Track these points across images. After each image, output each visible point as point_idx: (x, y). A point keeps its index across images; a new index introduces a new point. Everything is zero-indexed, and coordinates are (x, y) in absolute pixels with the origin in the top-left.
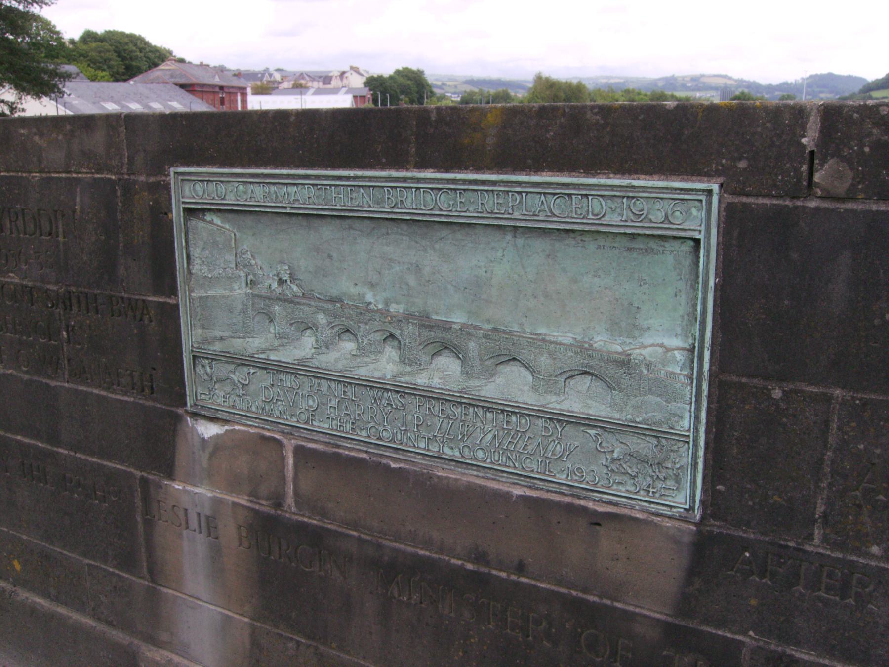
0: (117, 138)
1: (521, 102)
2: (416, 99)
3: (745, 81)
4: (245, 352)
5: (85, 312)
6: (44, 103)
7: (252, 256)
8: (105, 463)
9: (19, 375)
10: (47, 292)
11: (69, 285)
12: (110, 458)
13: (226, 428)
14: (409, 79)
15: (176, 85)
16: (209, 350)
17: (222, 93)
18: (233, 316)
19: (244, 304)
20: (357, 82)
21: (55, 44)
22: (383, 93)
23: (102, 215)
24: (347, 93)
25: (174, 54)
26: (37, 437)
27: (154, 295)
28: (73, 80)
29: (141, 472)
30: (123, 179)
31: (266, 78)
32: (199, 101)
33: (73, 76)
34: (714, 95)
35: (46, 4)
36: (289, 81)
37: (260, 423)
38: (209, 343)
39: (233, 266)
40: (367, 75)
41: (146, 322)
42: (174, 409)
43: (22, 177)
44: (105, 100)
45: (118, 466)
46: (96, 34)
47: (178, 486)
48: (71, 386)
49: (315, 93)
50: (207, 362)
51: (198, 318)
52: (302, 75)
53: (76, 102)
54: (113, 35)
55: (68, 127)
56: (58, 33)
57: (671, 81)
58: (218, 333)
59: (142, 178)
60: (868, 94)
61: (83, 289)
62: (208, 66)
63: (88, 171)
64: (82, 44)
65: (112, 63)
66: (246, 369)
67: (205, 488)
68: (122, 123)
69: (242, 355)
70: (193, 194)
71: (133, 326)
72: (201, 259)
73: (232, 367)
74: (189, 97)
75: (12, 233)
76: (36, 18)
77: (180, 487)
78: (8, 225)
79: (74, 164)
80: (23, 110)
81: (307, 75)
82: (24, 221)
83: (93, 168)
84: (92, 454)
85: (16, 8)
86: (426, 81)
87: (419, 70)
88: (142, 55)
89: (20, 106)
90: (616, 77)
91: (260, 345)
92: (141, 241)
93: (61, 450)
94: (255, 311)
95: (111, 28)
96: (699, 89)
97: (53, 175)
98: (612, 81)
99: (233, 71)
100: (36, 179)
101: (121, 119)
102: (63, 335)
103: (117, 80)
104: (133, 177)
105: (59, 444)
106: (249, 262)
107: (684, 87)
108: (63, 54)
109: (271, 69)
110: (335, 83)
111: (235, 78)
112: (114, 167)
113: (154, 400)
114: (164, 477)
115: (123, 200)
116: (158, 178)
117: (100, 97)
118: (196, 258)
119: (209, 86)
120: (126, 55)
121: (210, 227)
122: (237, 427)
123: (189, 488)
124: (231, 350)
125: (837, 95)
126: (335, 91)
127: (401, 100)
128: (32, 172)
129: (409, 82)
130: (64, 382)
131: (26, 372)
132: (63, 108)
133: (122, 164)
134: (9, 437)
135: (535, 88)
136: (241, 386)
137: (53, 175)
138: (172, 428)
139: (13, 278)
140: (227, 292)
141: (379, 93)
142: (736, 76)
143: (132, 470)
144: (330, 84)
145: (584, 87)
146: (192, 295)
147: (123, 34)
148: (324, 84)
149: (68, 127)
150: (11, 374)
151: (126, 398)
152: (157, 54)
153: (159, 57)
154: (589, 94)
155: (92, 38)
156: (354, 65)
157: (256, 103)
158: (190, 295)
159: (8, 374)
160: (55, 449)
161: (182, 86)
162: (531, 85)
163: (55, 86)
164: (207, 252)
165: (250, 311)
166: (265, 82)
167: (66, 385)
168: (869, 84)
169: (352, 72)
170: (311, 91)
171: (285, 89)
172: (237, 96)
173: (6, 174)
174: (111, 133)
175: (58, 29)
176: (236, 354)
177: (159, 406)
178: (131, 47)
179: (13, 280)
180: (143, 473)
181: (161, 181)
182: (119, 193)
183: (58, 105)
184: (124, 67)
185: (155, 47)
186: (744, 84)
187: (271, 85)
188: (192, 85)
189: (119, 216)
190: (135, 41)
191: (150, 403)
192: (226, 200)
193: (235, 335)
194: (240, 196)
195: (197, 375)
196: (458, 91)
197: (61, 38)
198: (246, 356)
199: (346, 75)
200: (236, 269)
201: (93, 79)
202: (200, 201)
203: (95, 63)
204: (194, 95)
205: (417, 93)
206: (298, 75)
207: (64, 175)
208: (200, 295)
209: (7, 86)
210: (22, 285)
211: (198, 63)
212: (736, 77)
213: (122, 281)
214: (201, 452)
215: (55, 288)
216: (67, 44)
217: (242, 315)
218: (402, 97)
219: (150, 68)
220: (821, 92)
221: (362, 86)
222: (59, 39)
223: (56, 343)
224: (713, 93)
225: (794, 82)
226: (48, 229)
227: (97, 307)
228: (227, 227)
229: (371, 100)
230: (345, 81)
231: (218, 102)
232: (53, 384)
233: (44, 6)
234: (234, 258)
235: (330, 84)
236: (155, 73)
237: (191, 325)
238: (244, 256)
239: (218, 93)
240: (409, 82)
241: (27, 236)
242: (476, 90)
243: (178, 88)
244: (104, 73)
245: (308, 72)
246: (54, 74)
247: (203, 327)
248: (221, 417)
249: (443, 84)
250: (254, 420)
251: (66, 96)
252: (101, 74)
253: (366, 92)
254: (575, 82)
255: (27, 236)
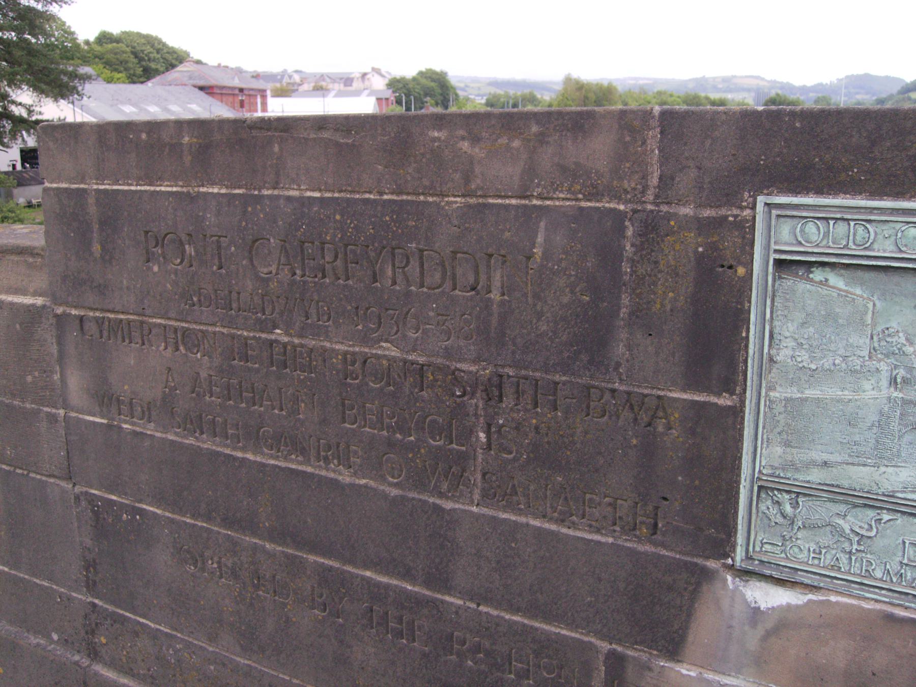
0: (641, 146)
1: (550, 105)
2: (440, 102)
3: (779, 82)
4: (875, 487)
5: (529, 407)
6: (61, 108)
7: (907, 339)
8: (537, 625)
9: (382, 488)
10: (453, 373)
11: (503, 366)
12: (548, 617)
13: (811, 596)
14: (433, 80)
15: (195, 86)
16: (794, 479)
17: (242, 96)
18: (856, 430)
19: (881, 413)
20: (379, 84)
21: (70, 45)
22: (408, 95)
23: (589, 264)
24: (368, 95)
25: (191, 56)
26: (407, 574)
27: (684, 390)
28: (93, 82)
29: (611, 644)
30: (644, 211)
31: (286, 80)
32: (219, 103)
33: (93, 77)
34: (747, 96)
35: (66, 3)
36: (309, 83)
37: (893, 598)
38: (797, 470)
39: (865, 353)
40: (390, 77)
41: (660, 429)
42: (699, 561)
43: (426, 203)
44: (122, 103)
45: (564, 632)
46: (112, 34)
47: (685, 670)
48: (485, 511)
49: (336, 96)
50: (787, 496)
51: (778, 430)
52: (322, 77)
53: (94, 105)
54: (129, 36)
55: (535, 129)
56: (73, 33)
57: (701, 82)
58: (819, 456)
59: (687, 211)
60: (906, 95)
61: (531, 374)
62: (227, 67)
63: (573, 197)
64: (96, 46)
65: (130, 65)
66: (871, 513)
67: (745, 679)
68: (655, 123)
69: (868, 492)
70: (800, 239)
71: (630, 433)
72: (796, 340)
73: (842, 508)
74: (208, 100)
75: (394, 283)
76: (52, 18)
77: (692, 674)
78: (389, 272)
79: (538, 185)
80: (40, 113)
81: (328, 76)
82: (422, 265)
83: (580, 192)
84: (516, 610)
85: (33, 8)
86: (448, 82)
87: (442, 72)
88: (159, 56)
89: (37, 109)
90: (645, 79)
91: (909, 479)
92: (668, 307)
93: (448, 598)
94: (906, 426)
95: (127, 29)
96: (730, 91)
97: (491, 201)
98: (641, 82)
99: (250, 72)
100: (455, 206)
101: (653, 117)
102: (477, 437)
103: (134, 82)
104: (664, 208)
105: (449, 590)
106: (899, 349)
107: (715, 89)
108: (78, 55)
109: (290, 71)
110: (356, 85)
111: (254, 80)
112: (626, 192)
113: (655, 544)
114: (658, 656)
115: (638, 243)
116: (723, 211)
117: (117, 100)
118: (786, 338)
119: (229, 88)
120: (144, 56)
121: (824, 291)
122: (833, 598)
123: (710, 676)
124: (846, 483)
125: (873, 95)
126: (357, 93)
127: (427, 102)
128: (448, 196)
129: (433, 84)
130: (471, 503)
131: (396, 485)
132: (80, 111)
133: (645, 188)
134: (349, 572)
135: (565, 89)
136: (856, 539)
137: (491, 201)
138: (691, 588)
139: (388, 349)
140: (846, 392)
141: (403, 95)
142: (769, 77)
143: (593, 640)
144: (351, 85)
145: (615, 89)
146: (772, 394)
147: (139, 35)
148: (345, 85)
149: (535, 129)
150: (365, 486)
151: (597, 537)
152: (175, 56)
153: (176, 59)
154: (620, 96)
155: (108, 39)
156: (376, 66)
157: (278, 107)
158: (767, 395)
159: (360, 486)
160: (439, 596)
161: (202, 88)
162: (559, 88)
163: (75, 88)
164: (811, 329)
165: (895, 425)
166: (285, 84)
167: (474, 509)
168: (907, 84)
169: (374, 73)
170: (333, 93)
171: (306, 91)
172: (256, 98)
173: (394, 197)
174: (628, 139)
175: (72, 30)
176: (855, 490)
177: (664, 552)
178: (148, 49)
179: (387, 353)
180: (614, 646)
181: (729, 216)
182: (630, 232)
183: (76, 109)
184: (141, 69)
185: (172, 48)
186: (778, 85)
187: (291, 87)
188: (211, 87)
189: (626, 268)
190: (151, 41)
191: (648, 548)
192: (873, 250)
193: (856, 460)
194: (906, 246)
195: (760, 514)
196: (481, 92)
197: (77, 39)
198: (877, 494)
199: (368, 76)
200: (870, 357)
201: (109, 81)
202: (816, 250)
203: (111, 66)
204: (213, 97)
205: (441, 94)
206: (318, 76)
207: (514, 202)
208: (789, 395)
209: (25, 87)
210: (405, 361)
211: (216, 64)
212: (768, 78)
213: (618, 365)
214: (747, 628)
215: (473, 368)
216: (82, 44)
217: (875, 430)
218: (428, 99)
219: (167, 70)
220: (857, 93)
221: (385, 88)
222: (74, 40)
223: (464, 448)
224: (745, 95)
225: (829, 83)
226: (471, 279)
227: (555, 401)
228: (858, 291)
229: (394, 102)
230: (367, 83)
231: (237, 105)
232: (448, 505)
233: (64, 5)
234: (868, 341)
235: (351, 85)
236: (173, 75)
237: (762, 439)
238: (889, 339)
239: (237, 95)
240: (433, 84)
241: (425, 290)
242: (502, 92)
243: (197, 90)
244: (120, 75)
245: (332, 74)
246: (74, 76)
247: (787, 444)
248: (806, 581)
249: (467, 86)
250: (877, 590)
251: (85, 98)
252: (117, 75)
253: (389, 94)
254: (605, 84)
255: (425, 290)
